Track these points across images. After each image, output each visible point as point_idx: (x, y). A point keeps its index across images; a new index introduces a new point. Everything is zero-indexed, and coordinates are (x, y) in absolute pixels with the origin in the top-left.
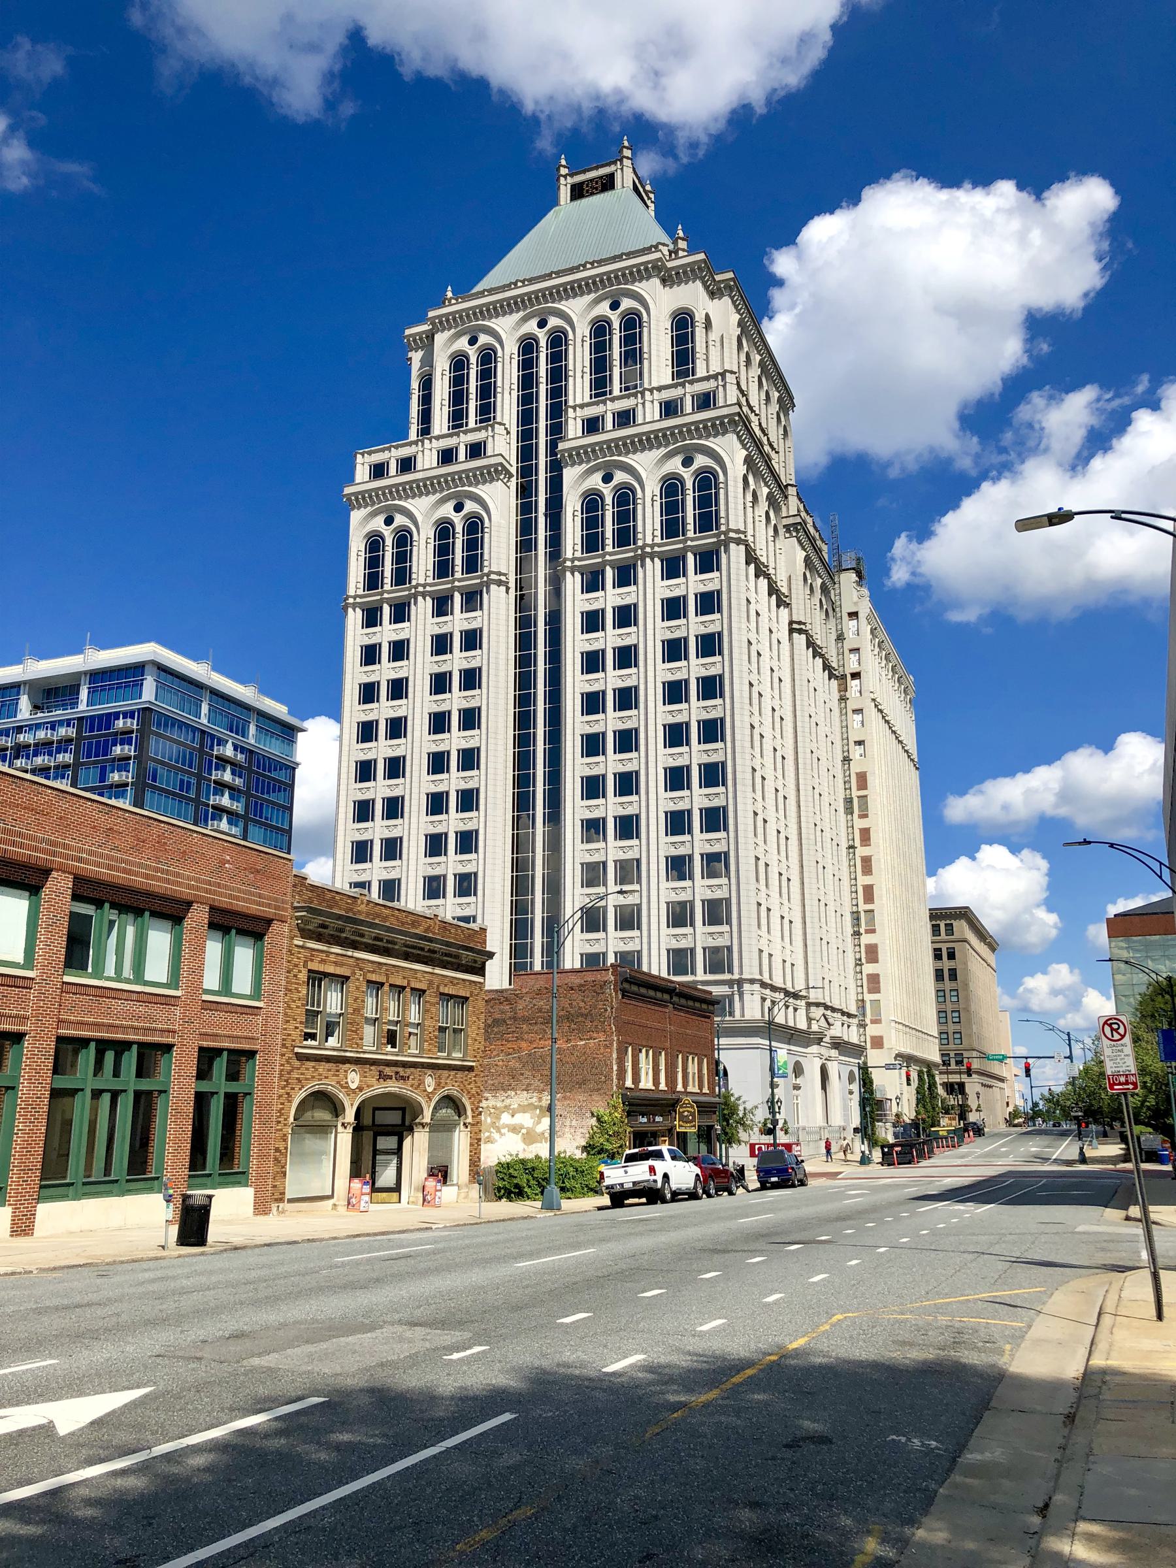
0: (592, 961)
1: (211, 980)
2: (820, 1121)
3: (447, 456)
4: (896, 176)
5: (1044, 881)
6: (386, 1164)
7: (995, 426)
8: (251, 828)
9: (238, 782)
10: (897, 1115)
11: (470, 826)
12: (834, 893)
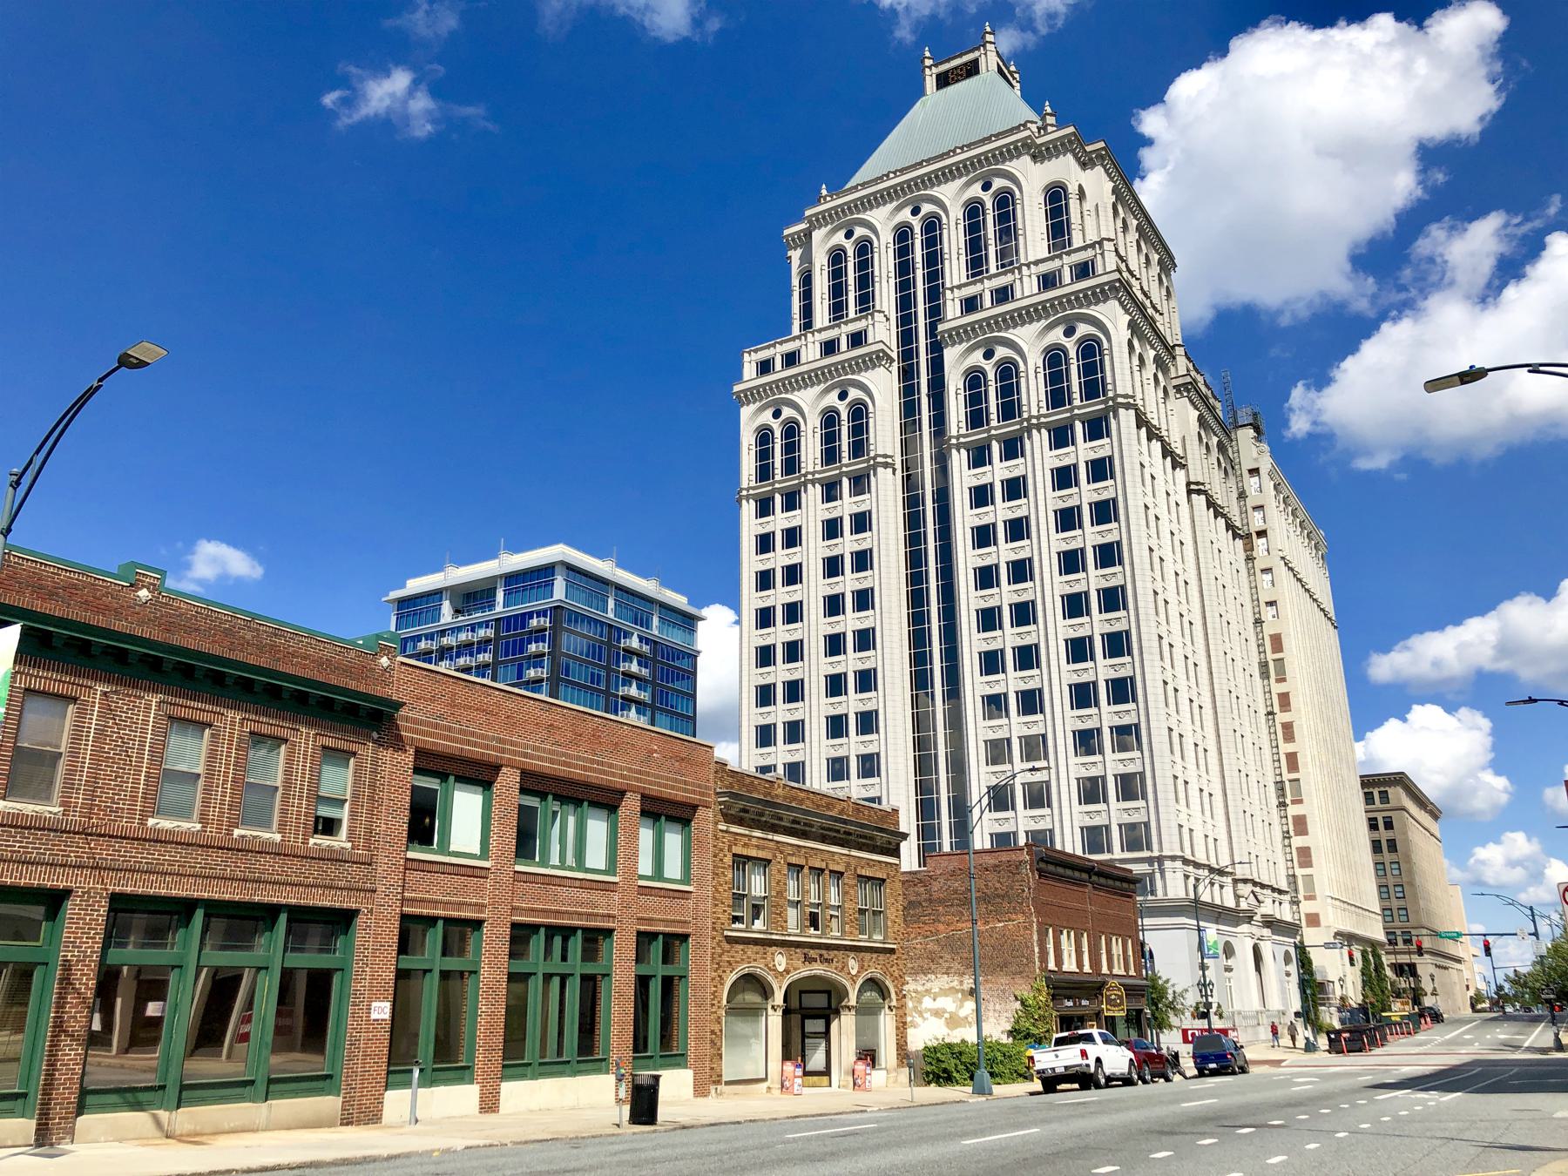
0: (1003, 840)
1: (645, 866)
2: (1256, 1005)
3: (830, 348)
4: (1265, 23)
5: (1488, 741)
6: (815, 1048)
7: (1393, 266)
8: (657, 716)
9: (645, 672)
10: (1342, 999)
11: (869, 707)
12: (1254, 762)
